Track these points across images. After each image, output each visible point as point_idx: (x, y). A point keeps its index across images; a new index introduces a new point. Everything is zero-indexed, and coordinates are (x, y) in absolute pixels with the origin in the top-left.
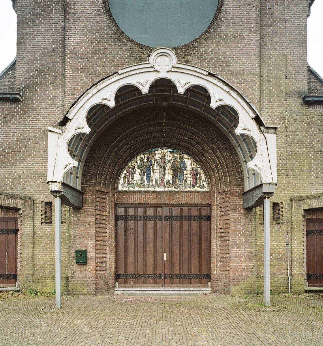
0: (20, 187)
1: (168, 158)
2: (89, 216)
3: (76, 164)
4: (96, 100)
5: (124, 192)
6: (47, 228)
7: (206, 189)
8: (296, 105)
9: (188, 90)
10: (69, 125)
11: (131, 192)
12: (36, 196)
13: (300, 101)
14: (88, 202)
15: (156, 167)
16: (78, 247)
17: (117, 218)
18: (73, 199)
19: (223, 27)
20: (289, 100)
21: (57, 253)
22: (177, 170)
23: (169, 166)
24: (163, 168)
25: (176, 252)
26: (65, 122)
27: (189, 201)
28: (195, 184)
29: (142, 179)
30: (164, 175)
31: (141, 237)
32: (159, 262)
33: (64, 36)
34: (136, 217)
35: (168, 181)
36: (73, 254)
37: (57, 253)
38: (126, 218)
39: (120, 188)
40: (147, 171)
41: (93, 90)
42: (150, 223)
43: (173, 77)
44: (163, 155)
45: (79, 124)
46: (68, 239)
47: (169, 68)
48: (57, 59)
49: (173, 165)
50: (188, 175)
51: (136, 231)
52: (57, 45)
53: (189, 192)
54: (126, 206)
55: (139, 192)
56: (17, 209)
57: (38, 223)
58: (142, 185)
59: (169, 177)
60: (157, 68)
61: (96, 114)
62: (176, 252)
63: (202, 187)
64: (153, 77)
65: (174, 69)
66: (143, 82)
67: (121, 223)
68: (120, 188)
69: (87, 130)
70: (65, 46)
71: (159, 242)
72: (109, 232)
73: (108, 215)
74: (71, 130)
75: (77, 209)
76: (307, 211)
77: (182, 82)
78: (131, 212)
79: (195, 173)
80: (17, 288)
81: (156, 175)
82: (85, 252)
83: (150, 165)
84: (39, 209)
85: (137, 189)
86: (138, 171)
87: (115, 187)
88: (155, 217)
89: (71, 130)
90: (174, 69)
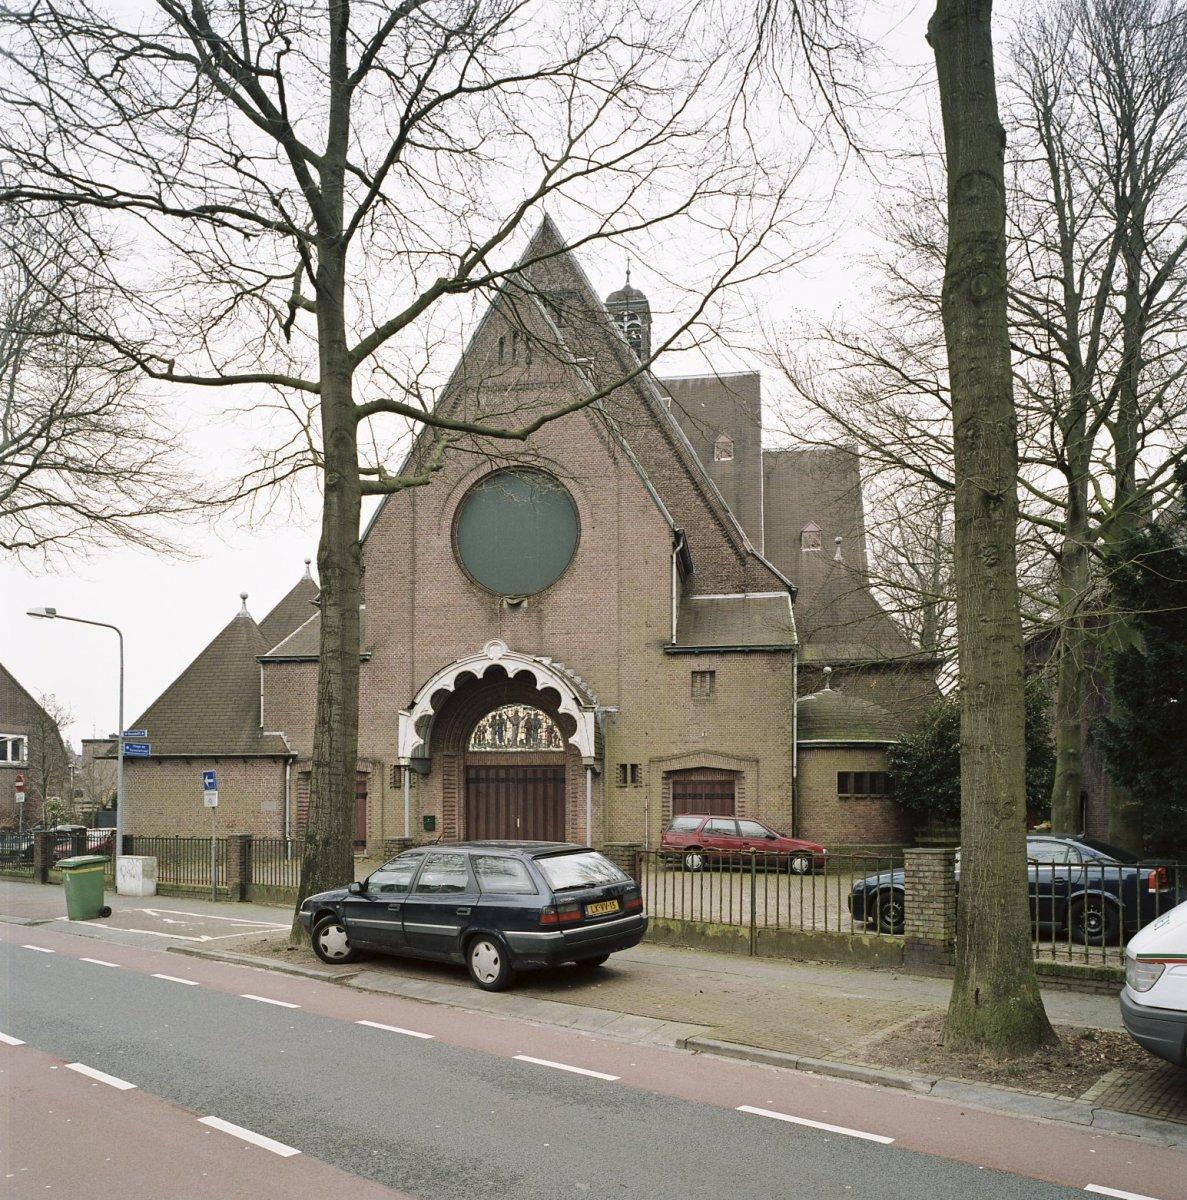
0: (369, 750)
1: (521, 715)
2: (437, 783)
3: (422, 742)
4: (438, 686)
5: (475, 753)
6: (397, 793)
7: (562, 749)
8: (656, 655)
9: (517, 675)
10: (416, 707)
11: (481, 753)
12: (384, 759)
13: (661, 651)
14: (436, 767)
15: (509, 725)
16: (426, 813)
17: (468, 782)
18: (422, 766)
19: (579, 571)
20: (649, 651)
21: (407, 819)
22: (532, 727)
23: (522, 723)
24: (516, 726)
25: (530, 818)
26: (412, 705)
27: (543, 763)
28: (550, 743)
29: (494, 739)
30: (517, 735)
31: (493, 801)
32: (512, 828)
33: (413, 590)
34: (487, 780)
35: (521, 740)
36: (421, 820)
37: (407, 819)
38: (477, 780)
39: (471, 749)
40: (498, 727)
41: (436, 678)
42: (502, 786)
43: (503, 663)
44: (517, 712)
45: (424, 707)
46: (417, 805)
47: (500, 655)
48: (405, 615)
49: (527, 722)
50: (543, 734)
51: (488, 795)
52: (405, 600)
53: (542, 752)
54: (478, 768)
55: (491, 752)
56: (366, 773)
57: (387, 787)
58: (494, 745)
59: (522, 736)
60: (491, 656)
61: (439, 697)
62: (530, 818)
63: (558, 746)
64: (487, 664)
65: (505, 657)
66: (478, 669)
67: (472, 786)
68: (471, 749)
69: (431, 712)
70: (413, 600)
71: (512, 808)
72: (458, 797)
73: (458, 779)
74: (418, 712)
75: (426, 775)
76: (669, 774)
77: (512, 668)
78: (483, 774)
79: (550, 730)
80: (366, 855)
81: (508, 734)
82: (843, 777)
83: (502, 723)
84: (388, 772)
85: (488, 749)
86: (490, 730)
87: (465, 749)
88: (507, 780)
89: (418, 712)
90: (505, 657)
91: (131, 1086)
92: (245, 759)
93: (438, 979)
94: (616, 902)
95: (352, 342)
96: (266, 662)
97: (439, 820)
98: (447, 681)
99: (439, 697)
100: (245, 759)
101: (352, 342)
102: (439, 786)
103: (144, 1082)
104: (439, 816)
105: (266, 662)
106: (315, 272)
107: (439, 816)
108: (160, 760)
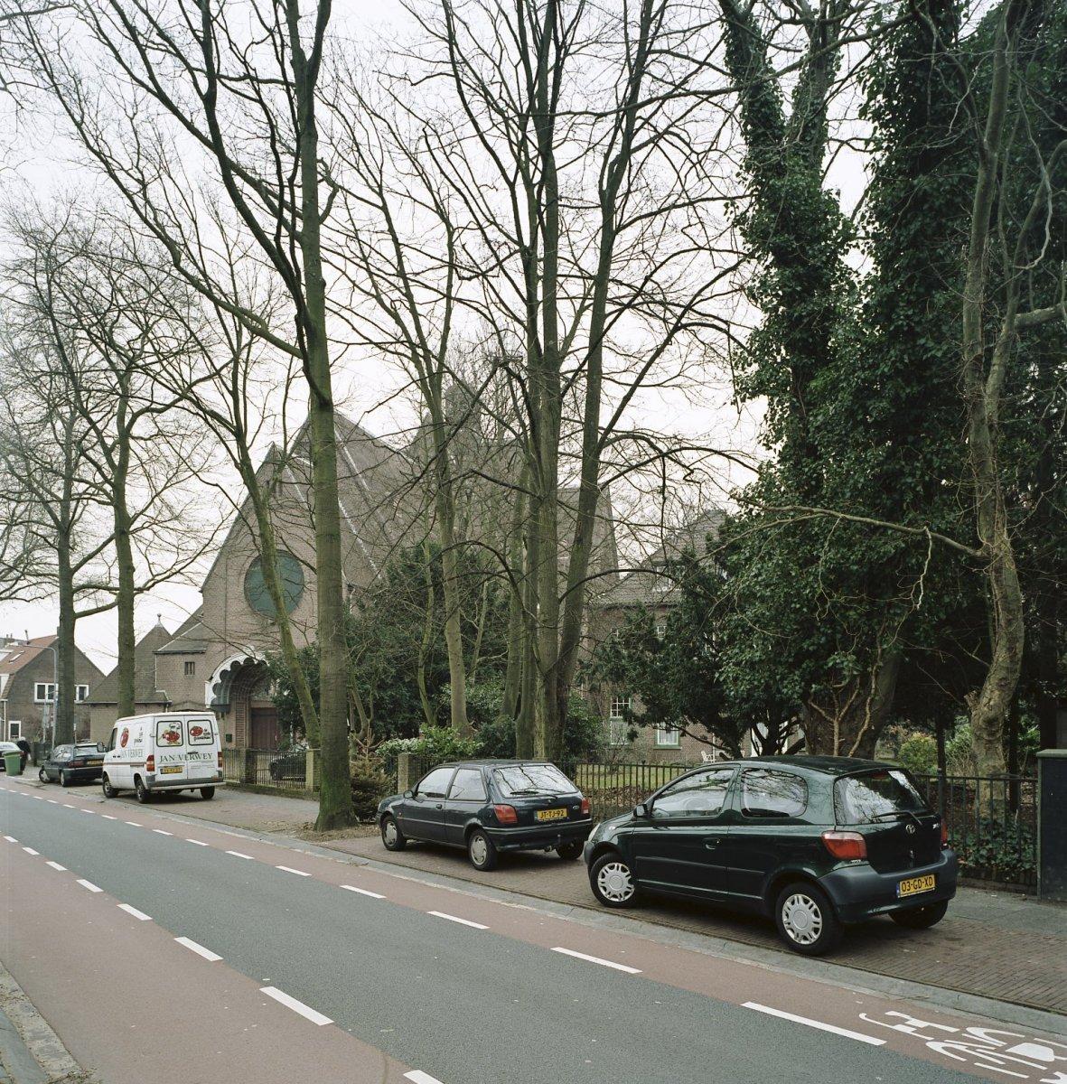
14: (233, 709)
45: (217, 679)
72: (246, 725)
73: (245, 715)
74: (214, 682)
89: (214, 682)
91: (99, 890)
92: (146, 705)
93: (707, 930)
94: (565, 810)
95: (512, 180)
96: (157, 654)
97: (234, 738)
98: (227, 666)
99: (224, 674)
100: (146, 705)
101: (512, 180)
102: (234, 718)
103: (229, 958)
104: (234, 734)
105: (157, 654)
106: (552, 42)
107: (234, 734)
108: (107, 705)
